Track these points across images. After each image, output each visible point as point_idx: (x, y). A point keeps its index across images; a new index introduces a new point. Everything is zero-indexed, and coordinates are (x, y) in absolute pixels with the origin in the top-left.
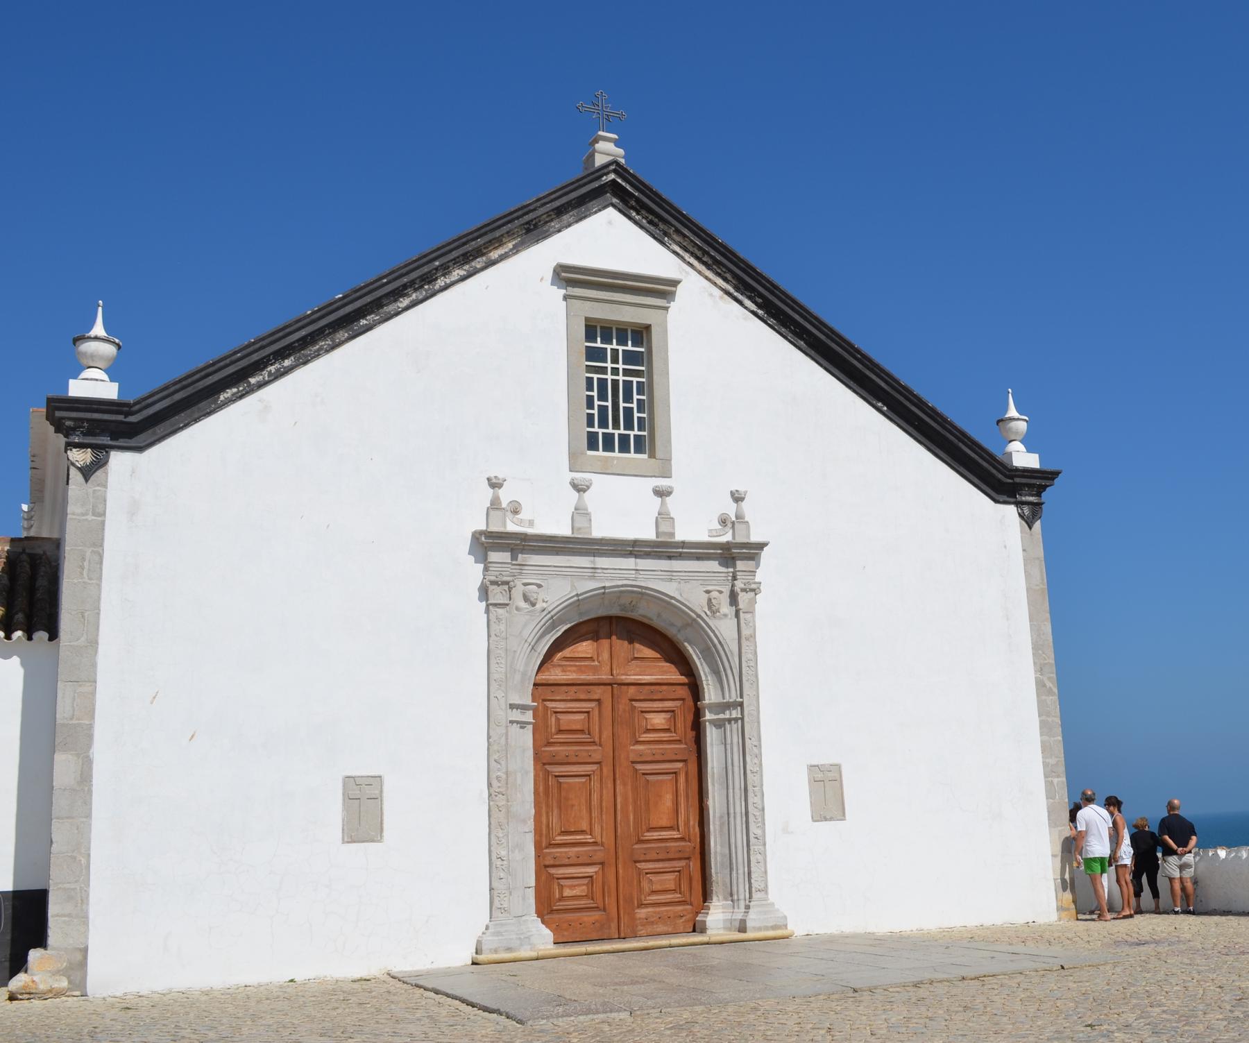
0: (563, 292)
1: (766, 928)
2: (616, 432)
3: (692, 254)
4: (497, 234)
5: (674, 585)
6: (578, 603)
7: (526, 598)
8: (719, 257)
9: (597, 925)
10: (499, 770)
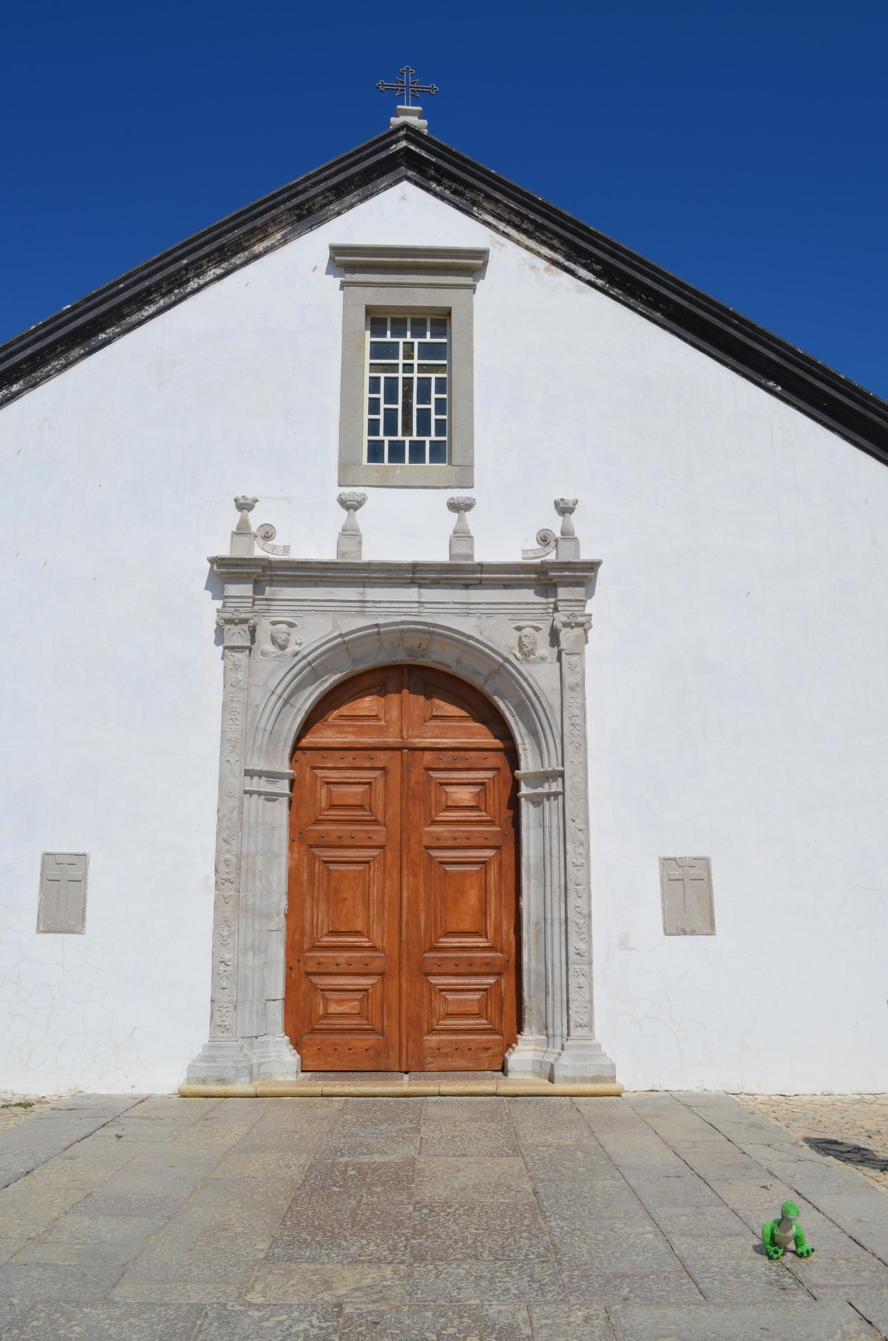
0: (338, 281)
1: (584, 1080)
2: (407, 439)
3: (509, 223)
4: (259, 222)
5: (472, 620)
6: (345, 646)
7: (274, 641)
8: (540, 220)
9: (372, 1052)
10: (228, 851)
